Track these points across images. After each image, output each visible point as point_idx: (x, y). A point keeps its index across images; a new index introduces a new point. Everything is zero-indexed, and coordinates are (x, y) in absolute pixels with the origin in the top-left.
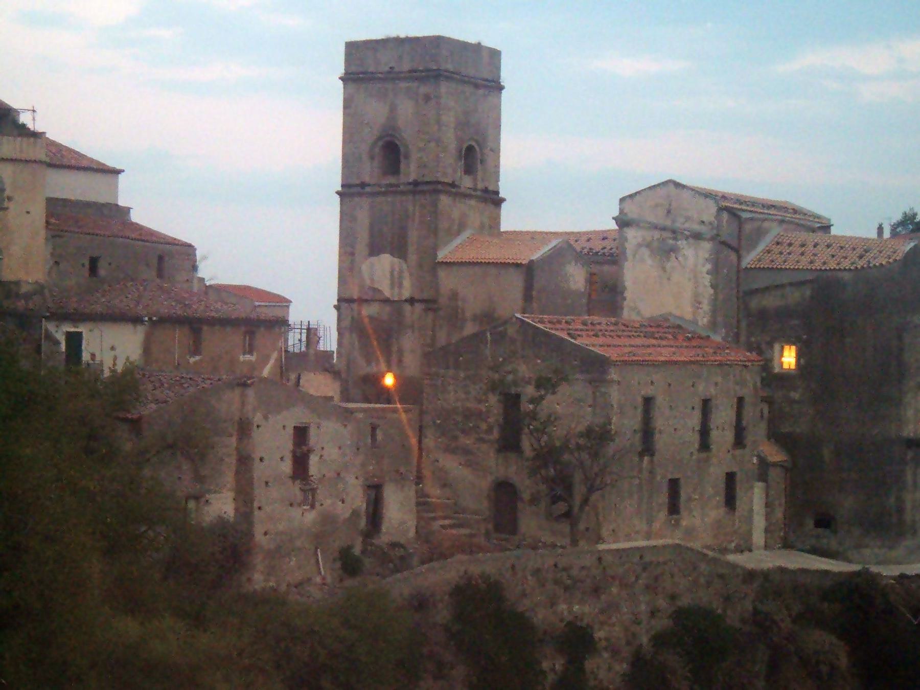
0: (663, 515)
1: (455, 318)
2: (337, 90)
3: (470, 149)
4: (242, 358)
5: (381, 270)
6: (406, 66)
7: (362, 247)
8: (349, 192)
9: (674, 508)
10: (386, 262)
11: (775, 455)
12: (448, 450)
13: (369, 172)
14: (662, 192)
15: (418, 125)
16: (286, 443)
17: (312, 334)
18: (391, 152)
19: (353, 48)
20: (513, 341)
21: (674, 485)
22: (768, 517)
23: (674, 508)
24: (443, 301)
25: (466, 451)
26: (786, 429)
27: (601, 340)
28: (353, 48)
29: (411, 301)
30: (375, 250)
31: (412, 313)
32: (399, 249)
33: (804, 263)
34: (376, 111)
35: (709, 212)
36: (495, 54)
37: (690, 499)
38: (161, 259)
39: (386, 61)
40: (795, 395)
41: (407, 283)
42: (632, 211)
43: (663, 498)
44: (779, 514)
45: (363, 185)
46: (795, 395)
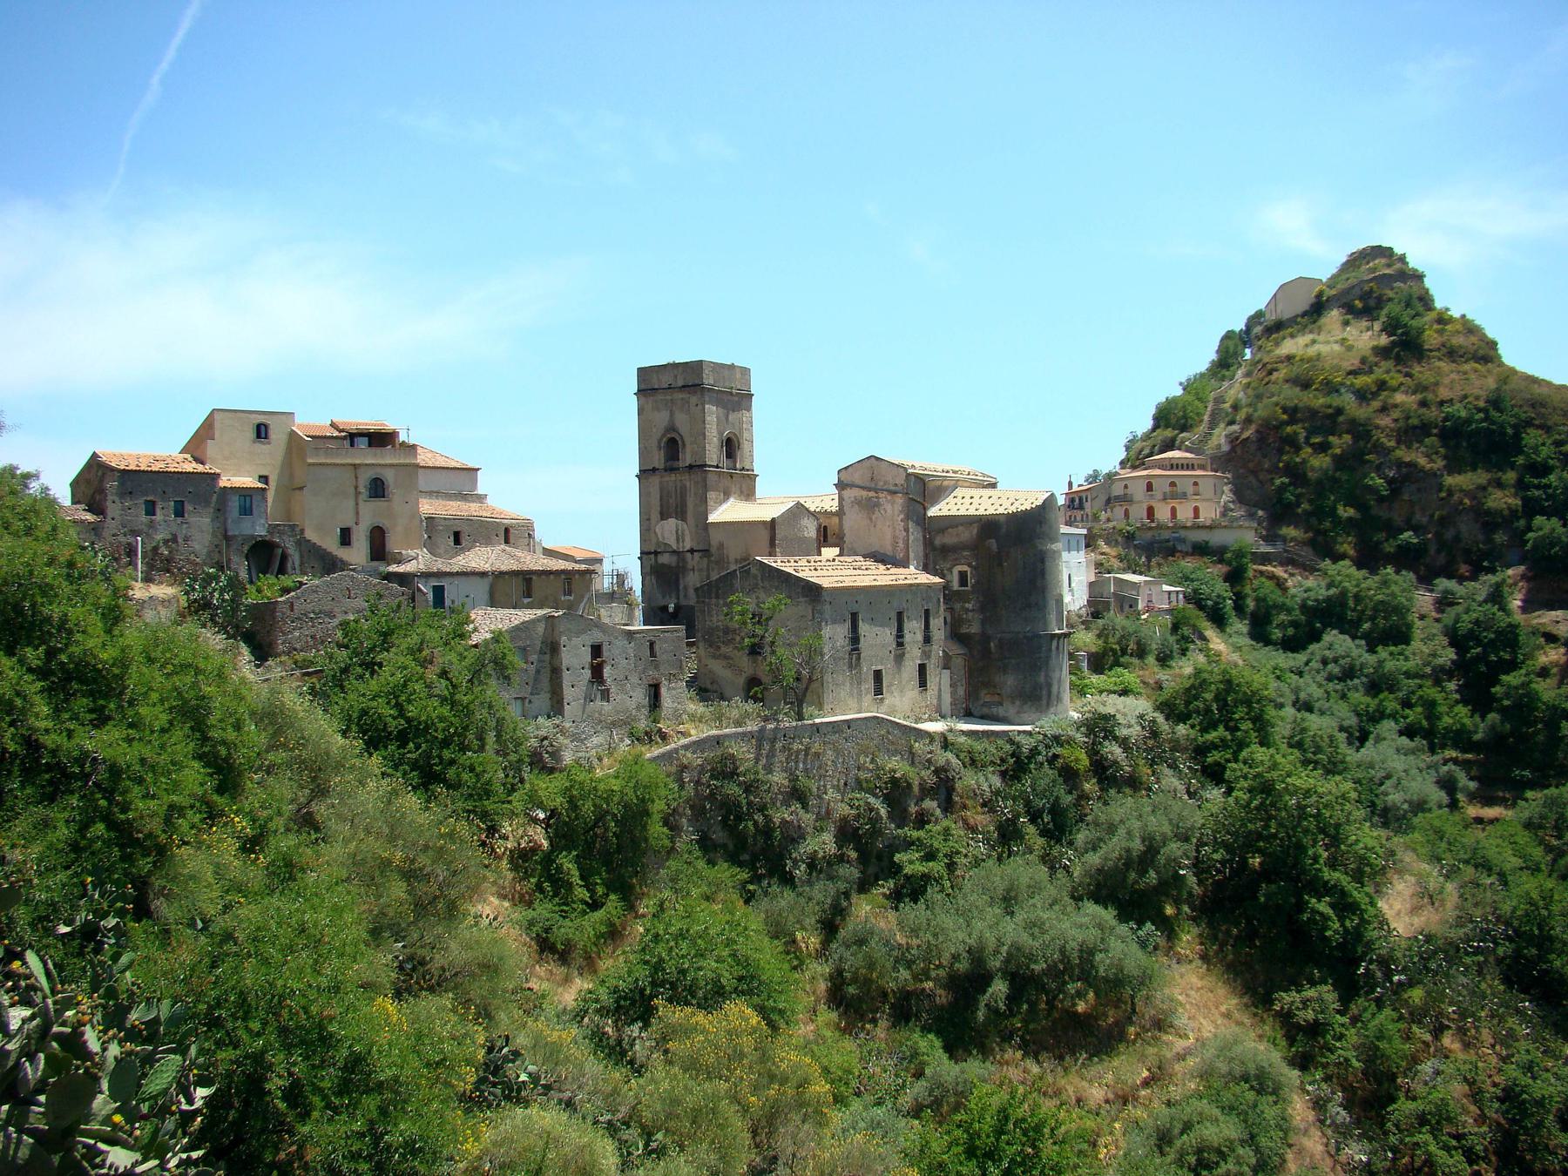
0: (870, 696)
1: (721, 561)
2: (633, 403)
3: (729, 441)
4: (139, 591)
5: (668, 529)
6: (680, 383)
7: (655, 515)
8: (645, 474)
9: (879, 691)
10: (672, 523)
11: (956, 649)
12: (714, 657)
13: (658, 460)
14: (867, 464)
15: (687, 422)
16: (586, 656)
17: (621, 578)
18: (672, 446)
19: (642, 372)
20: (755, 577)
21: (878, 675)
22: (953, 694)
23: (879, 691)
24: (713, 550)
25: (726, 657)
26: (964, 630)
27: (819, 573)
28: (642, 372)
29: (692, 551)
30: (664, 516)
31: (693, 561)
32: (681, 514)
33: (972, 512)
34: (661, 419)
35: (901, 480)
36: (745, 372)
37: (891, 685)
38: (507, 530)
39: (666, 380)
40: (969, 606)
41: (687, 538)
42: (846, 478)
43: (870, 684)
44: (961, 691)
45: (654, 470)
46: (969, 606)
